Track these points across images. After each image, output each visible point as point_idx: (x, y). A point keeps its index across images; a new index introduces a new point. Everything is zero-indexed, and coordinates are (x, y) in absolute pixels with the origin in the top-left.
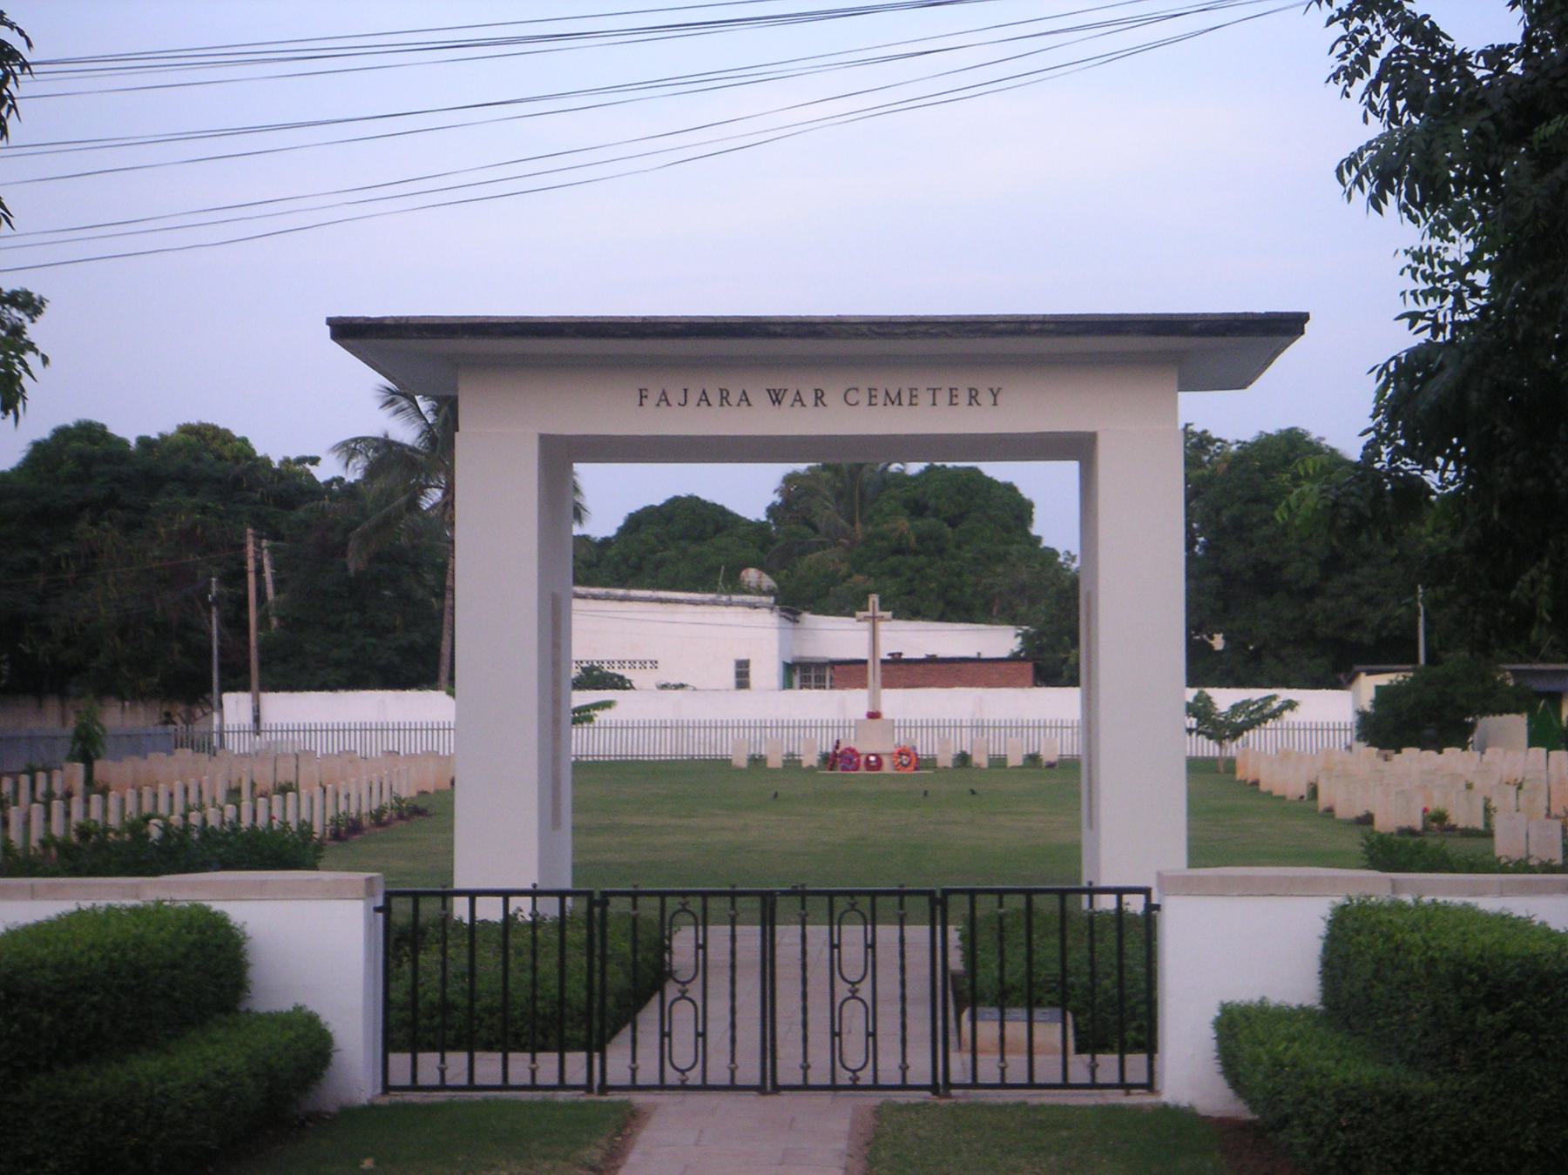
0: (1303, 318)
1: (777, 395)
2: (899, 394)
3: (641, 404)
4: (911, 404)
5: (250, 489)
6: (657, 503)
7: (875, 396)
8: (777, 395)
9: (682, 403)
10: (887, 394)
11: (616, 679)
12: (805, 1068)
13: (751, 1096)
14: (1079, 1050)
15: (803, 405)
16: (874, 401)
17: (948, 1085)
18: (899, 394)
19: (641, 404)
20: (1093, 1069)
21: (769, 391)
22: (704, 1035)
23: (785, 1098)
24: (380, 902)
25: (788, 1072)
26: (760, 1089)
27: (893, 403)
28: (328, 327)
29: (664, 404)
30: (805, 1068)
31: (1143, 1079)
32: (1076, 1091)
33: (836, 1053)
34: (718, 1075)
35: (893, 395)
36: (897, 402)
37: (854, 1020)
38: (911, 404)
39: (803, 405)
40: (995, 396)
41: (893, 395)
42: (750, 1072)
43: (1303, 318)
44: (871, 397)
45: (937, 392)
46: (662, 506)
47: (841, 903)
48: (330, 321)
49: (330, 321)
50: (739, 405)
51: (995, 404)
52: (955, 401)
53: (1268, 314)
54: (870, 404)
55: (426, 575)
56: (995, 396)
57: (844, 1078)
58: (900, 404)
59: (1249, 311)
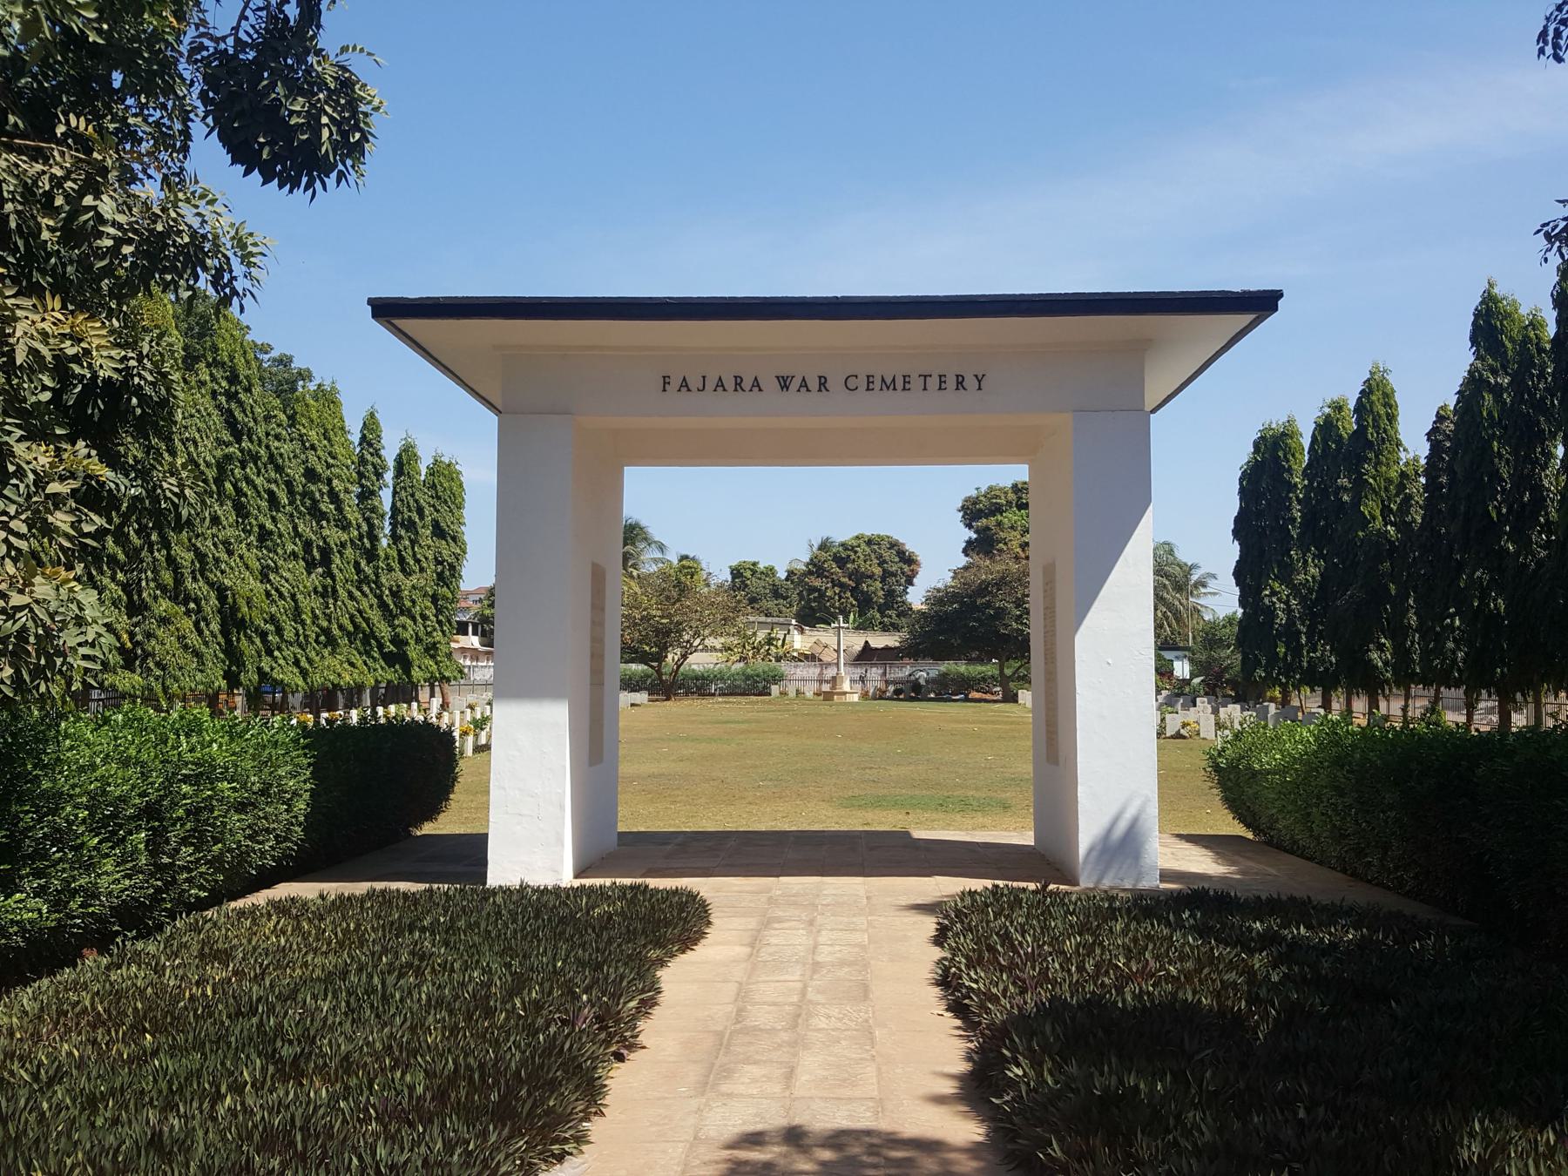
0: (1278, 295)
1: (785, 382)
2: (894, 379)
3: (664, 390)
4: (904, 389)
6: (1237, 558)
7: (909, 382)
8: (785, 382)
9: (701, 388)
10: (883, 380)
11: (956, 642)
15: (724, 390)
16: (907, 386)
18: (894, 379)
19: (664, 390)
21: (778, 377)
27: (888, 388)
28: (370, 308)
29: (720, 389)
32: (973, 704)
35: (889, 381)
36: (892, 387)
38: (904, 389)
39: (808, 390)
40: (979, 381)
41: (889, 381)
43: (1278, 295)
44: (868, 383)
45: (928, 378)
46: (1240, 556)
48: (371, 302)
49: (371, 302)
50: (751, 390)
51: (980, 389)
52: (943, 386)
53: (1244, 292)
54: (868, 389)
56: (979, 381)
58: (895, 389)
59: (1262, 289)
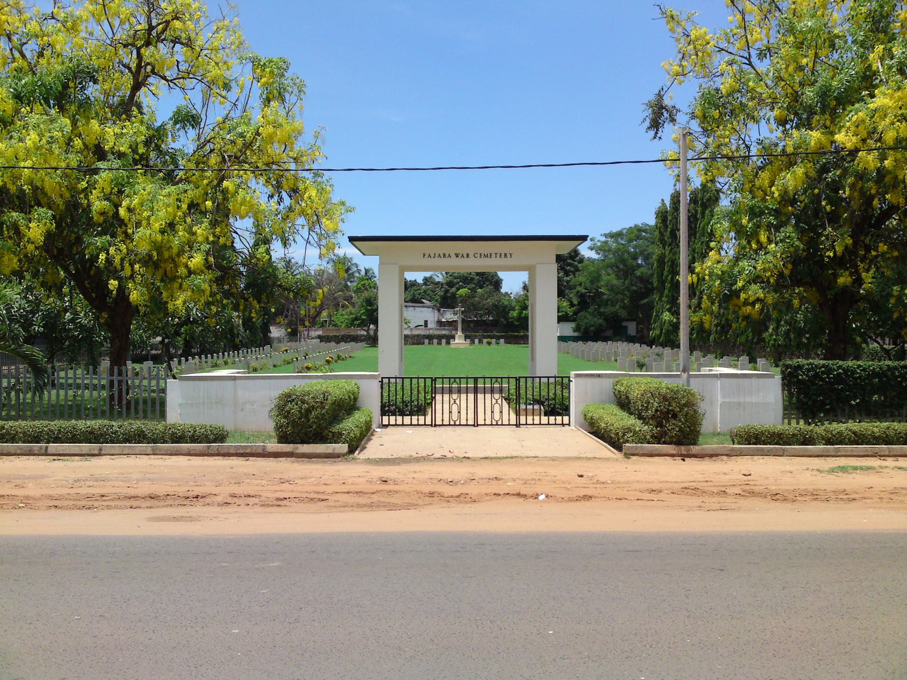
5: (879, 109)
12: (443, 420)
13: (472, 428)
14: (545, 415)
17: (520, 424)
20: (396, 420)
22: (492, 412)
23: (437, 428)
24: (380, 380)
25: (481, 422)
26: (474, 425)
30: (443, 420)
31: (568, 423)
33: (492, 417)
34: (463, 422)
37: (455, 408)
42: (471, 422)
47: (452, 380)
48: (349, 237)
49: (349, 237)
55: (776, 195)
57: (452, 423)
